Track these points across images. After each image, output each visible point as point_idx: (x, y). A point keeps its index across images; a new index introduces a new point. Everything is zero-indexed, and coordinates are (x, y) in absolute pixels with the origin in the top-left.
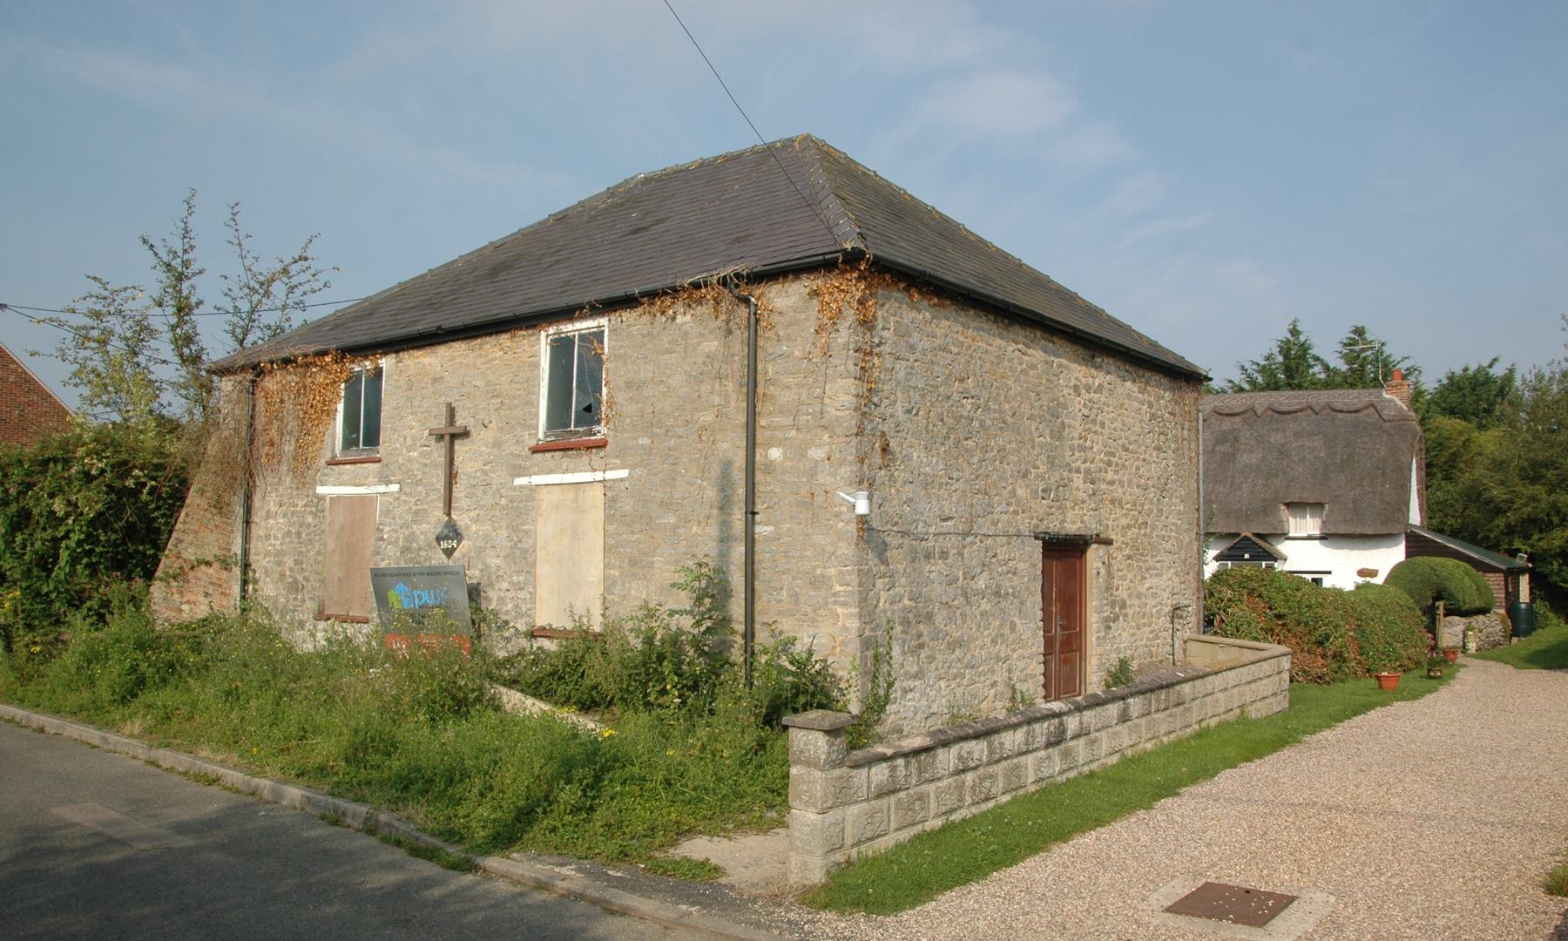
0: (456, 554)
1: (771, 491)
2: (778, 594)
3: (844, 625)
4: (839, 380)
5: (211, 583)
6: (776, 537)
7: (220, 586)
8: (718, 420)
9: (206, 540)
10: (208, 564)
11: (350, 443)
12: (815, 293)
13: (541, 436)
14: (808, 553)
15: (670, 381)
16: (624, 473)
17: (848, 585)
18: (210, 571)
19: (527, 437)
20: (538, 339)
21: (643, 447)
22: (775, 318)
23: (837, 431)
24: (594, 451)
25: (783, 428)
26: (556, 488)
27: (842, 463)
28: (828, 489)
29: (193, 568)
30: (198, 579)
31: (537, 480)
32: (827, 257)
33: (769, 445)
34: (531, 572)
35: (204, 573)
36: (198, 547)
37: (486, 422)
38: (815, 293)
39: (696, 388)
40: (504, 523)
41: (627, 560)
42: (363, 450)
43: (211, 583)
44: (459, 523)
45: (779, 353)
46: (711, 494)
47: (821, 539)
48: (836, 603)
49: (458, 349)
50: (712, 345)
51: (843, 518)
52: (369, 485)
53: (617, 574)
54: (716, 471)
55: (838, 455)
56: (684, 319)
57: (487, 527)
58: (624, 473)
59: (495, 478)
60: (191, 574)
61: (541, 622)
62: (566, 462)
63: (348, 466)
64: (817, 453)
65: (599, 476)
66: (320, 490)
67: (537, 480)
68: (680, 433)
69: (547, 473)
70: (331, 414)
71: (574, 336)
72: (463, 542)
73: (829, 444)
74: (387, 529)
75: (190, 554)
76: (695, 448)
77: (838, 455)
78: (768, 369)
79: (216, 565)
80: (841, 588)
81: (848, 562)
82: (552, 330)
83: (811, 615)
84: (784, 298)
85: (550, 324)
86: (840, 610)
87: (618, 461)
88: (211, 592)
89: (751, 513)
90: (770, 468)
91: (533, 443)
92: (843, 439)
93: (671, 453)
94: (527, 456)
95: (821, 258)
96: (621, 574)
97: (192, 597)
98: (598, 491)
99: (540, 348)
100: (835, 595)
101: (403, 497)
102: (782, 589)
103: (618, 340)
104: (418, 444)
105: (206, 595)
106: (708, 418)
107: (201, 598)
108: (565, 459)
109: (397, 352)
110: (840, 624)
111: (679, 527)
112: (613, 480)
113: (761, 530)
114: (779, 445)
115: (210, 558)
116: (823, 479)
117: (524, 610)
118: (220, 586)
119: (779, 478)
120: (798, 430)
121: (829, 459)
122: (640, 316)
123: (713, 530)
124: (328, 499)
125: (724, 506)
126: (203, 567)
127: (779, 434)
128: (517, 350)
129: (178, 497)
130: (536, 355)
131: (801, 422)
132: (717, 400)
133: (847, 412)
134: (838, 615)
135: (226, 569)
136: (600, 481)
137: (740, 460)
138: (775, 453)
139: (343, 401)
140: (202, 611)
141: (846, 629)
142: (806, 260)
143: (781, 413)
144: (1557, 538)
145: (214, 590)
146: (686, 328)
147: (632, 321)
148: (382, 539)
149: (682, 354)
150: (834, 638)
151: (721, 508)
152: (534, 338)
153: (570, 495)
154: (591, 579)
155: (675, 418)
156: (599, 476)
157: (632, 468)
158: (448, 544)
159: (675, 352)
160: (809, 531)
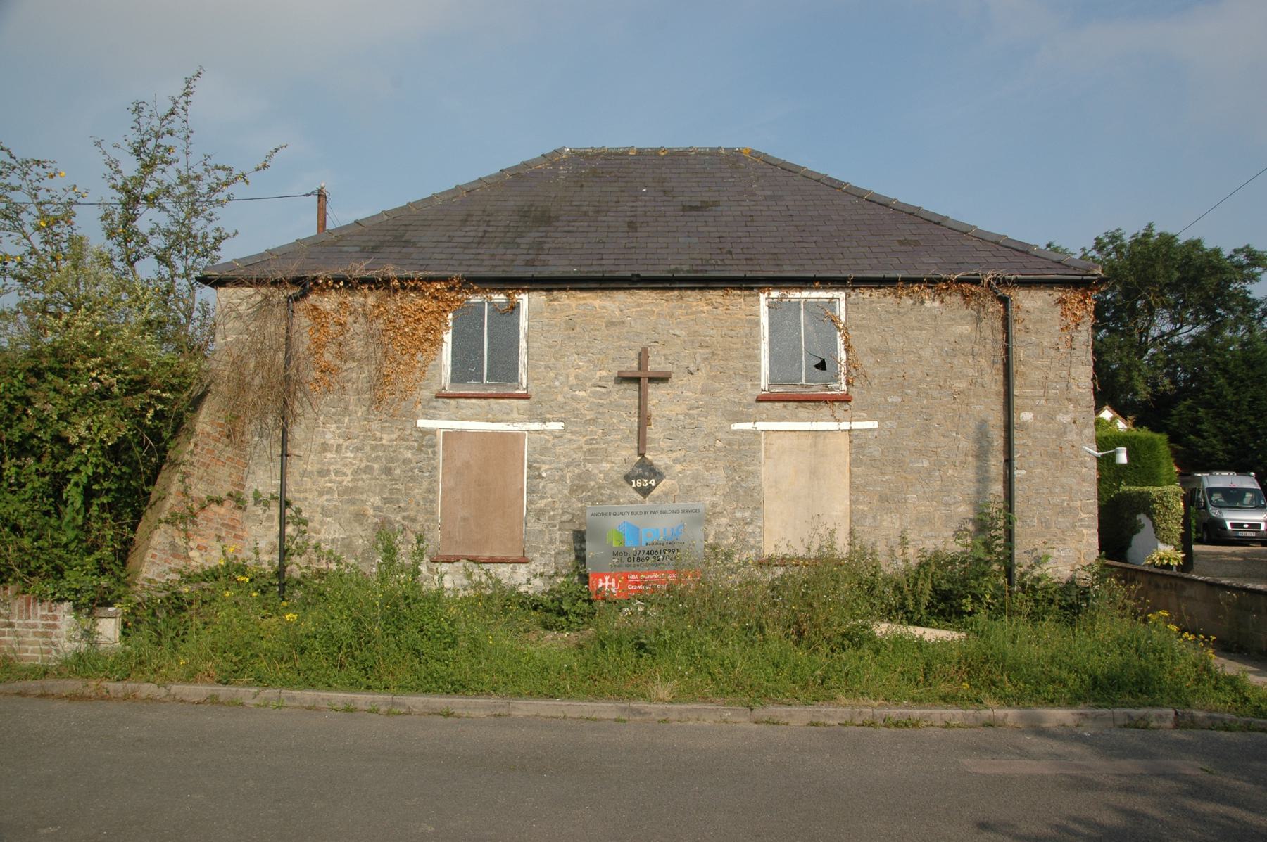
0: (655, 492)
1: (1024, 444)
2: (1031, 521)
3: (1087, 541)
4: (1080, 367)
5: (224, 525)
6: (1029, 478)
7: (234, 528)
8: (972, 387)
9: (217, 475)
10: (219, 502)
11: (458, 376)
12: (1061, 301)
13: (764, 383)
14: (1057, 490)
15: (922, 353)
16: (873, 425)
17: (1090, 513)
18: (222, 510)
19: (749, 387)
20: (759, 300)
21: (894, 404)
22: (1021, 315)
23: (1081, 403)
24: (837, 404)
25: (1033, 398)
26: (789, 434)
27: (1086, 425)
28: (1074, 444)
29: (203, 508)
30: (209, 520)
31: (761, 426)
32: (1085, 278)
33: (1024, 408)
34: (758, 507)
35: (215, 513)
36: (210, 482)
37: (692, 369)
38: (1061, 301)
39: (949, 360)
40: (721, 464)
41: (876, 497)
42: (487, 384)
43: (224, 525)
44: (654, 463)
45: (1029, 341)
46: (966, 444)
47: (1068, 480)
48: (1082, 526)
49: (648, 299)
50: (966, 329)
51: (1087, 465)
52: (513, 421)
53: (866, 509)
54: (971, 428)
55: (1082, 420)
56: (934, 304)
57: (698, 467)
58: (873, 425)
59: (708, 423)
60: (201, 515)
61: (769, 550)
62: (802, 412)
63: (473, 401)
64: (1064, 418)
65: (845, 425)
66: (423, 423)
67: (761, 426)
68: (935, 395)
69: (779, 421)
70: (437, 343)
71: (799, 303)
72: (664, 481)
73: (1073, 411)
74: (545, 467)
75: (200, 490)
76: (948, 408)
77: (1082, 420)
78: (1020, 353)
79: (229, 504)
80: (1085, 516)
81: (1090, 497)
82: (775, 294)
83: (1060, 535)
84: (1030, 302)
85: (775, 288)
86: (1085, 531)
87: (865, 415)
88: (223, 534)
89: (1009, 462)
90: (1024, 427)
91: (758, 393)
92: (1085, 409)
93: (924, 410)
94: (750, 405)
95: (1080, 278)
96: (871, 509)
97: (202, 542)
98: (844, 440)
99: (759, 308)
100: (1081, 520)
101: (569, 436)
102: (1033, 517)
103: (859, 313)
104: (588, 384)
105: (219, 538)
106: (961, 385)
107: (214, 543)
108: (800, 409)
109: (549, 290)
110: (1084, 541)
111: (934, 470)
112: (860, 430)
113: (1018, 473)
114: (1031, 410)
115: (224, 496)
116: (1072, 436)
117: (752, 542)
118: (234, 528)
119: (1032, 434)
120: (1046, 400)
121: (1074, 423)
122: (885, 295)
123: (970, 473)
124: (440, 435)
125: (982, 454)
126: (214, 507)
127: (1030, 402)
128: (731, 307)
129: (179, 424)
130: (757, 314)
131: (1050, 395)
132: (971, 372)
133: (1088, 390)
134: (1083, 535)
135: (240, 508)
136: (845, 430)
137: (996, 418)
138: (1026, 416)
139: (451, 331)
140: (215, 559)
141: (1089, 544)
142: (660, 286)
143: (1033, 386)
144: (2, 620)
145: (227, 533)
146: (935, 311)
147: (875, 298)
148: (540, 476)
149: (933, 332)
150: (1080, 551)
151: (977, 457)
152: (752, 299)
153: (809, 441)
154: (835, 513)
155: (928, 383)
156: (845, 425)
157: (881, 421)
158: (642, 482)
159: (925, 330)
160: (1059, 474)
